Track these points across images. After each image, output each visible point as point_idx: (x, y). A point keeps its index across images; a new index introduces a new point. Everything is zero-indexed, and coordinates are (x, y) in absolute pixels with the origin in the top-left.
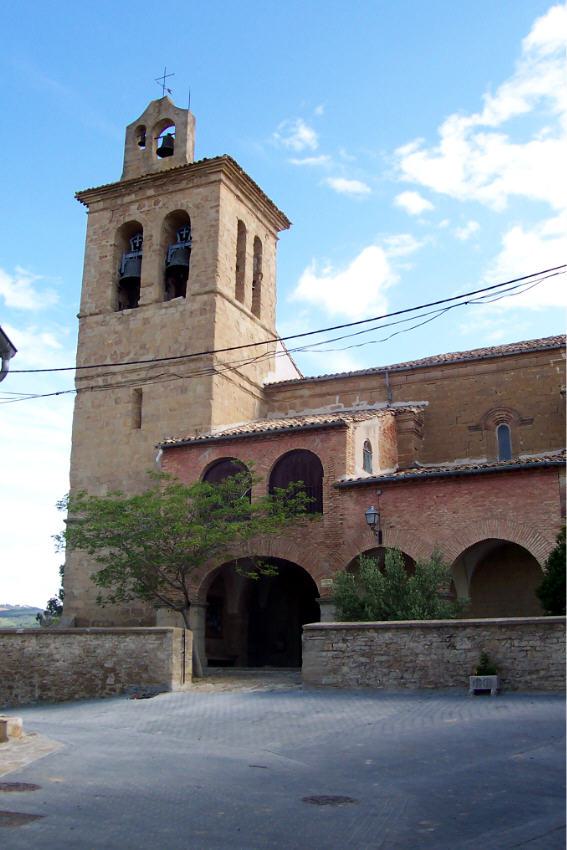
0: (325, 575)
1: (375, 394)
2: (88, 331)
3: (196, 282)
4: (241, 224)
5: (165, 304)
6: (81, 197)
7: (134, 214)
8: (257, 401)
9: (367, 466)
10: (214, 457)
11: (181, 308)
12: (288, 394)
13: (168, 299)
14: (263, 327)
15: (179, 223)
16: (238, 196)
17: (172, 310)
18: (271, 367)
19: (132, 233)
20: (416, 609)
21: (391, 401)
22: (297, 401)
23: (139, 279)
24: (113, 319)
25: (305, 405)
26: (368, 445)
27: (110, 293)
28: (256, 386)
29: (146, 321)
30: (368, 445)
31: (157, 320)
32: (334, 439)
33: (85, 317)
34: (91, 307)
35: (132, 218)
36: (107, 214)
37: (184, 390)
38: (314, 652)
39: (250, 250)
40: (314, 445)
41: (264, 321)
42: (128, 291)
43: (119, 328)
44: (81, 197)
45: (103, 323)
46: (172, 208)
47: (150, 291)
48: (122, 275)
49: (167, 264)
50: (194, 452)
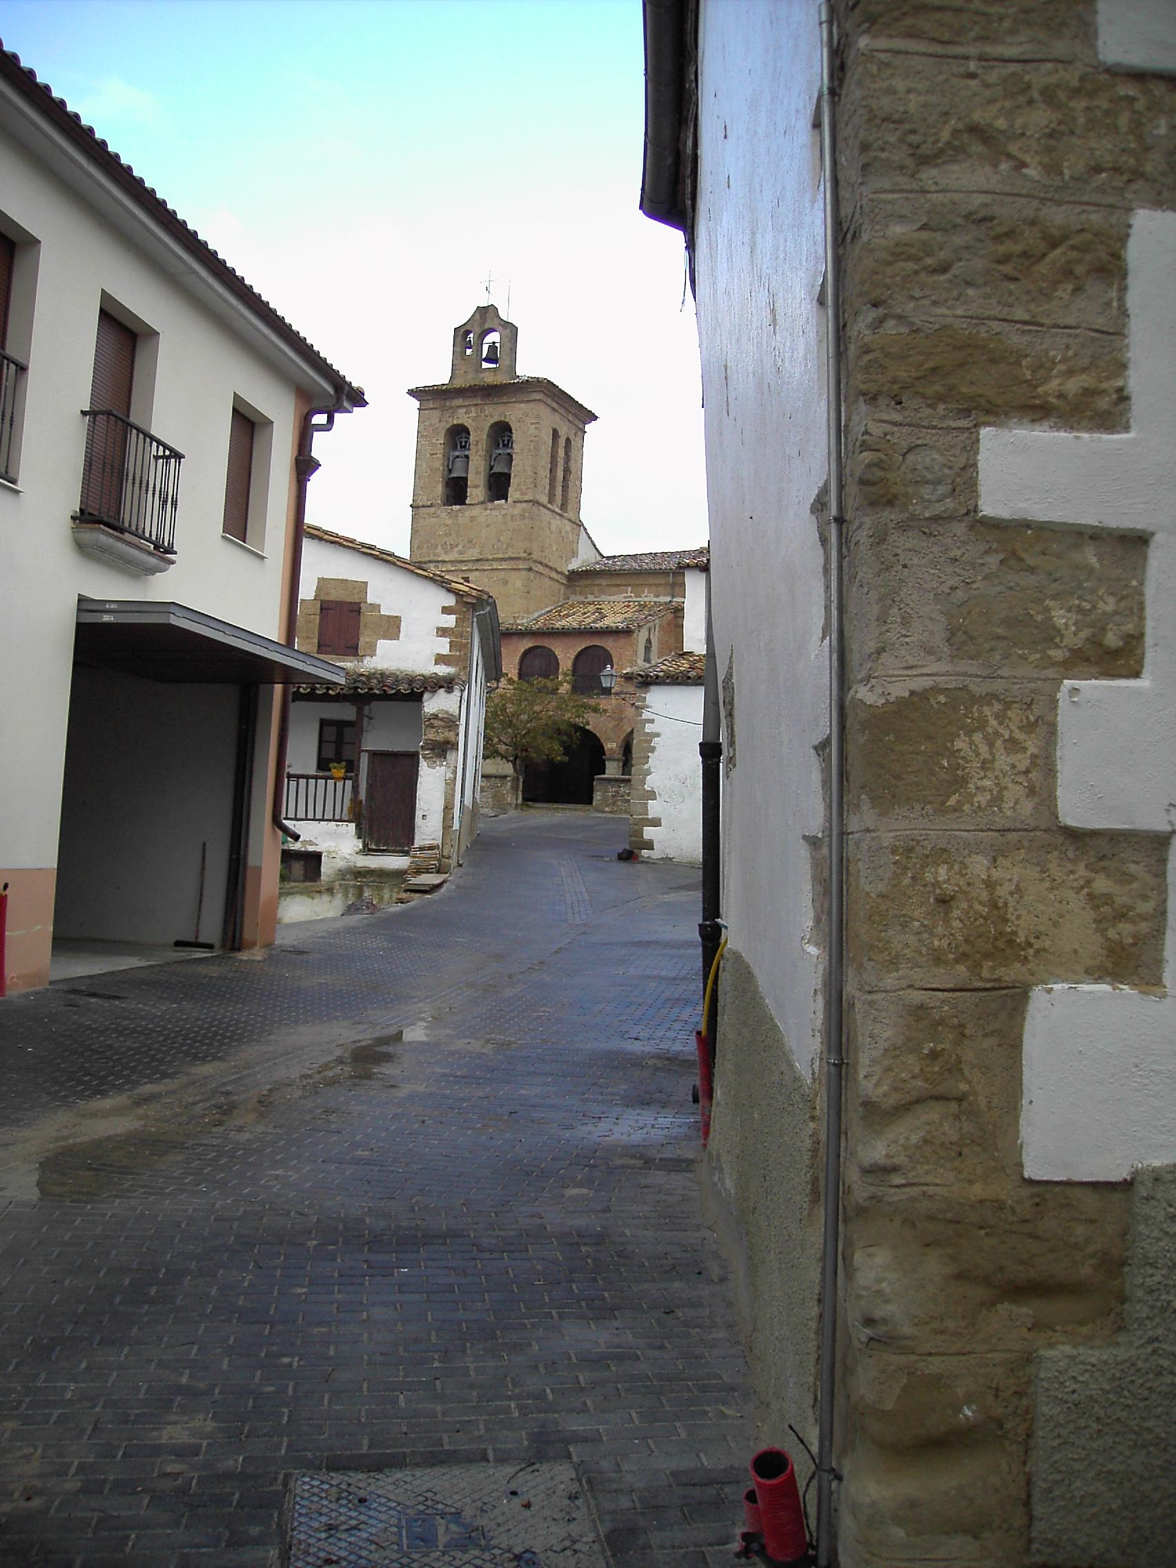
0: (609, 740)
1: (661, 589)
2: (421, 521)
3: (516, 490)
4: (555, 434)
5: (490, 505)
6: (411, 393)
7: (462, 417)
8: (563, 588)
9: (647, 660)
10: (531, 645)
11: (503, 512)
12: (588, 582)
13: (492, 501)
14: (570, 520)
15: (501, 433)
16: (554, 409)
17: (495, 513)
18: (574, 554)
19: (458, 436)
20: (451, 735)
21: (673, 597)
22: (596, 589)
23: (466, 478)
24: (443, 512)
25: (602, 592)
26: (649, 641)
27: (439, 489)
28: (561, 573)
29: (473, 519)
30: (649, 641)
31: (482, 519)
32: (623, 641)
33: (418, 507)
34: (423, 500)
35: (460, 422)
36: (437, 413)
37: (505, 583)
38: (597, 796)
39: (561, 453)
40: (608, 644)
41: (570, 515)
42: (456, 491)
43: (449, 522)
44: (411, 393)
45: (435, 515)
46: (496, 419)
47: (477, 491)
48: (450, 471)
49: (491, 468)
50: (514, 640)
